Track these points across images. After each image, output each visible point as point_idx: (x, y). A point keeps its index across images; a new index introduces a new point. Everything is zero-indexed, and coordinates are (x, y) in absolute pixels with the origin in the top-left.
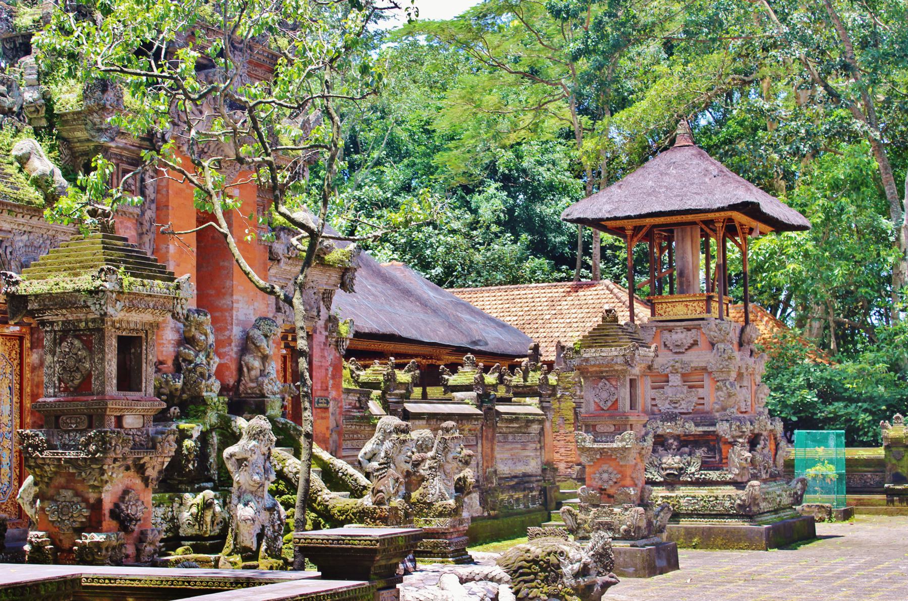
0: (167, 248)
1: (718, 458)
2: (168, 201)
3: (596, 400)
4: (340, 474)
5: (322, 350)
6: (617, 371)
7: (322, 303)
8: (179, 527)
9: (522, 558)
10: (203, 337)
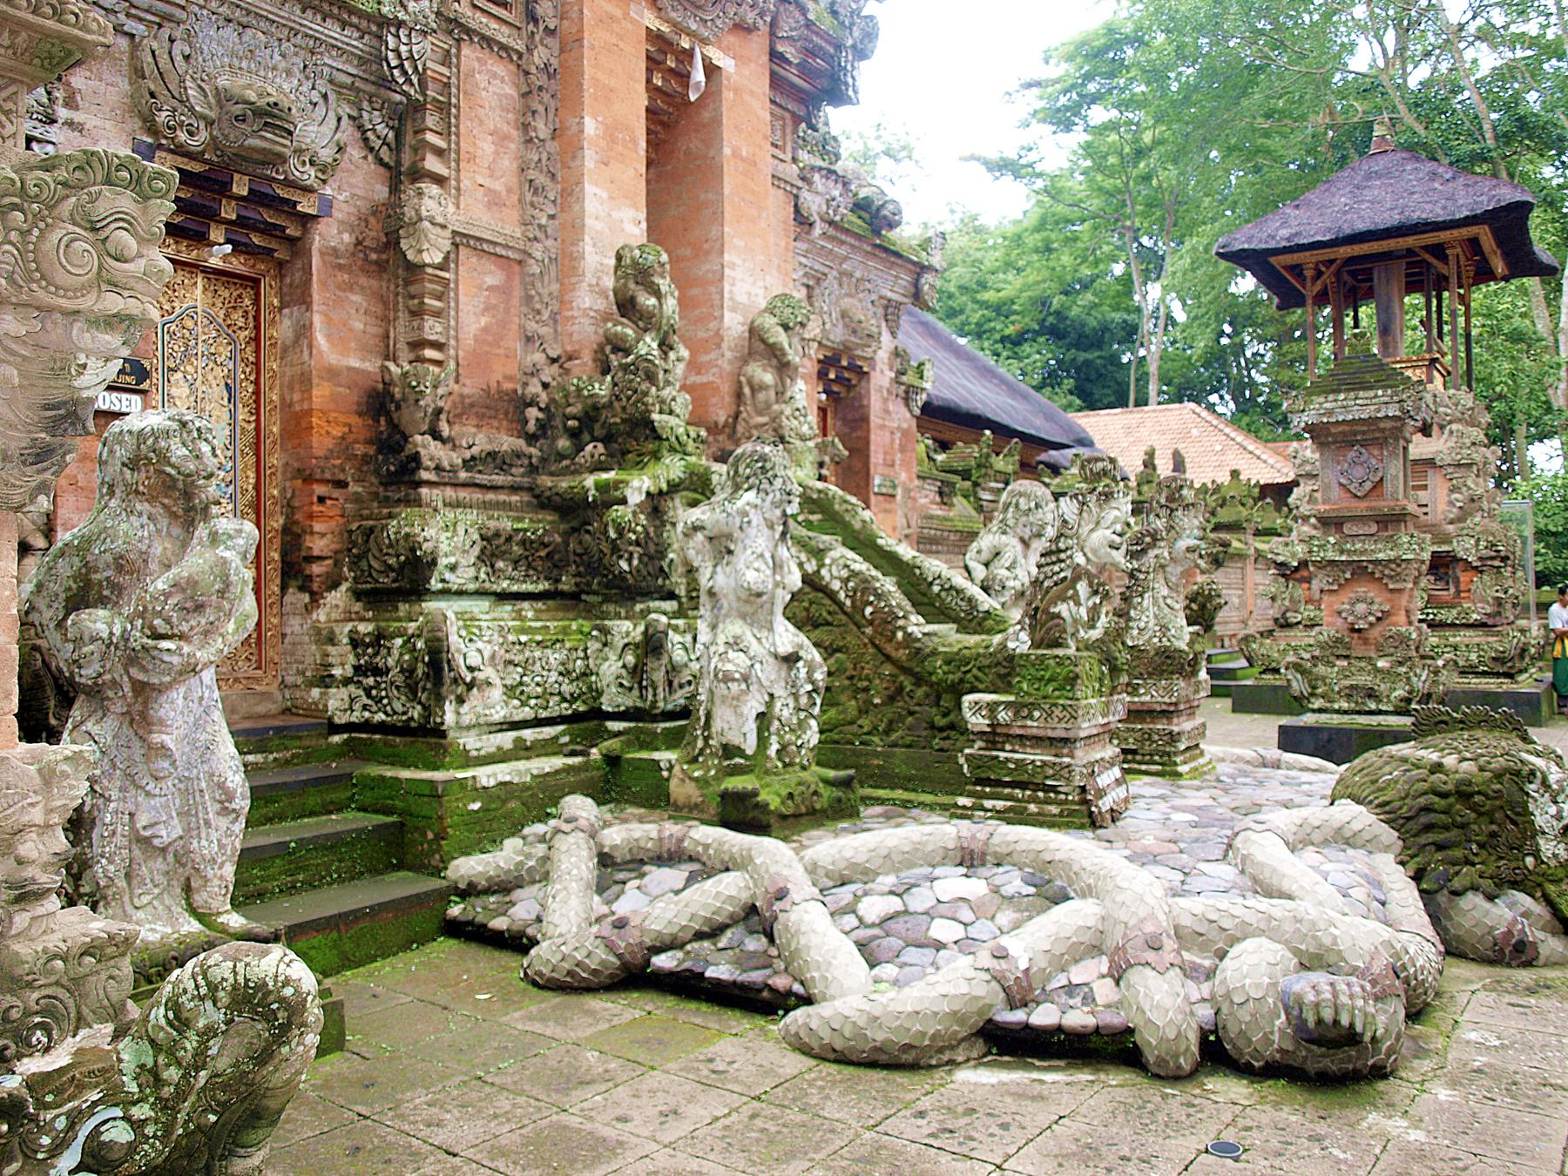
0: (581, 124)
1: (1452, 590)
2: (581, 31)
3: (1343, 481)
4: (936, 589)
5: (885, 401)
6: (1383, 430)
7: (884, 324)
8: (600, 693)
9: (1425, 786)
10: (653, 301)
